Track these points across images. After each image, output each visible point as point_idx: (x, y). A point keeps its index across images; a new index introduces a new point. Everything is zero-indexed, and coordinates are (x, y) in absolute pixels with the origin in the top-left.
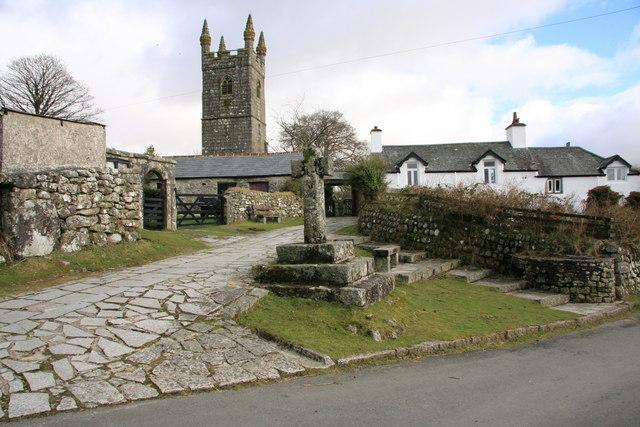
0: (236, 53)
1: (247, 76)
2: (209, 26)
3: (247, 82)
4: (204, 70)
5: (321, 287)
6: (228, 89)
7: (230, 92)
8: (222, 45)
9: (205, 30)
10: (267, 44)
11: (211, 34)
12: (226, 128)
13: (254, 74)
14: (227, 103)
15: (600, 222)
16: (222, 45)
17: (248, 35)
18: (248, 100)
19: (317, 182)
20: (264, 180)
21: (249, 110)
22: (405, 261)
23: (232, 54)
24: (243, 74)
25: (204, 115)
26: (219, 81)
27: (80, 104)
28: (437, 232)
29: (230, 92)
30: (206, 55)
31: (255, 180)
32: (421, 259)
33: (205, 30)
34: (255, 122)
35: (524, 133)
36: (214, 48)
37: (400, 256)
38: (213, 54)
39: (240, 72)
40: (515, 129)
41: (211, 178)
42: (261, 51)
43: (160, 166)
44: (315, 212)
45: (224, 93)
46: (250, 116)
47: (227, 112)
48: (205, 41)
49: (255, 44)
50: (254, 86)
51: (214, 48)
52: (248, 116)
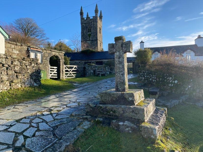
0: (92, 18)
4: (81, 24)
7: (90, 31)
8: (87, 15)
16: (87, 15)
17: (96, 11)
23: (91, 18)
30: (82, 19)
36: (85, 16)
45: (89, 32)
48: (81, 14)
51: (85, 16)
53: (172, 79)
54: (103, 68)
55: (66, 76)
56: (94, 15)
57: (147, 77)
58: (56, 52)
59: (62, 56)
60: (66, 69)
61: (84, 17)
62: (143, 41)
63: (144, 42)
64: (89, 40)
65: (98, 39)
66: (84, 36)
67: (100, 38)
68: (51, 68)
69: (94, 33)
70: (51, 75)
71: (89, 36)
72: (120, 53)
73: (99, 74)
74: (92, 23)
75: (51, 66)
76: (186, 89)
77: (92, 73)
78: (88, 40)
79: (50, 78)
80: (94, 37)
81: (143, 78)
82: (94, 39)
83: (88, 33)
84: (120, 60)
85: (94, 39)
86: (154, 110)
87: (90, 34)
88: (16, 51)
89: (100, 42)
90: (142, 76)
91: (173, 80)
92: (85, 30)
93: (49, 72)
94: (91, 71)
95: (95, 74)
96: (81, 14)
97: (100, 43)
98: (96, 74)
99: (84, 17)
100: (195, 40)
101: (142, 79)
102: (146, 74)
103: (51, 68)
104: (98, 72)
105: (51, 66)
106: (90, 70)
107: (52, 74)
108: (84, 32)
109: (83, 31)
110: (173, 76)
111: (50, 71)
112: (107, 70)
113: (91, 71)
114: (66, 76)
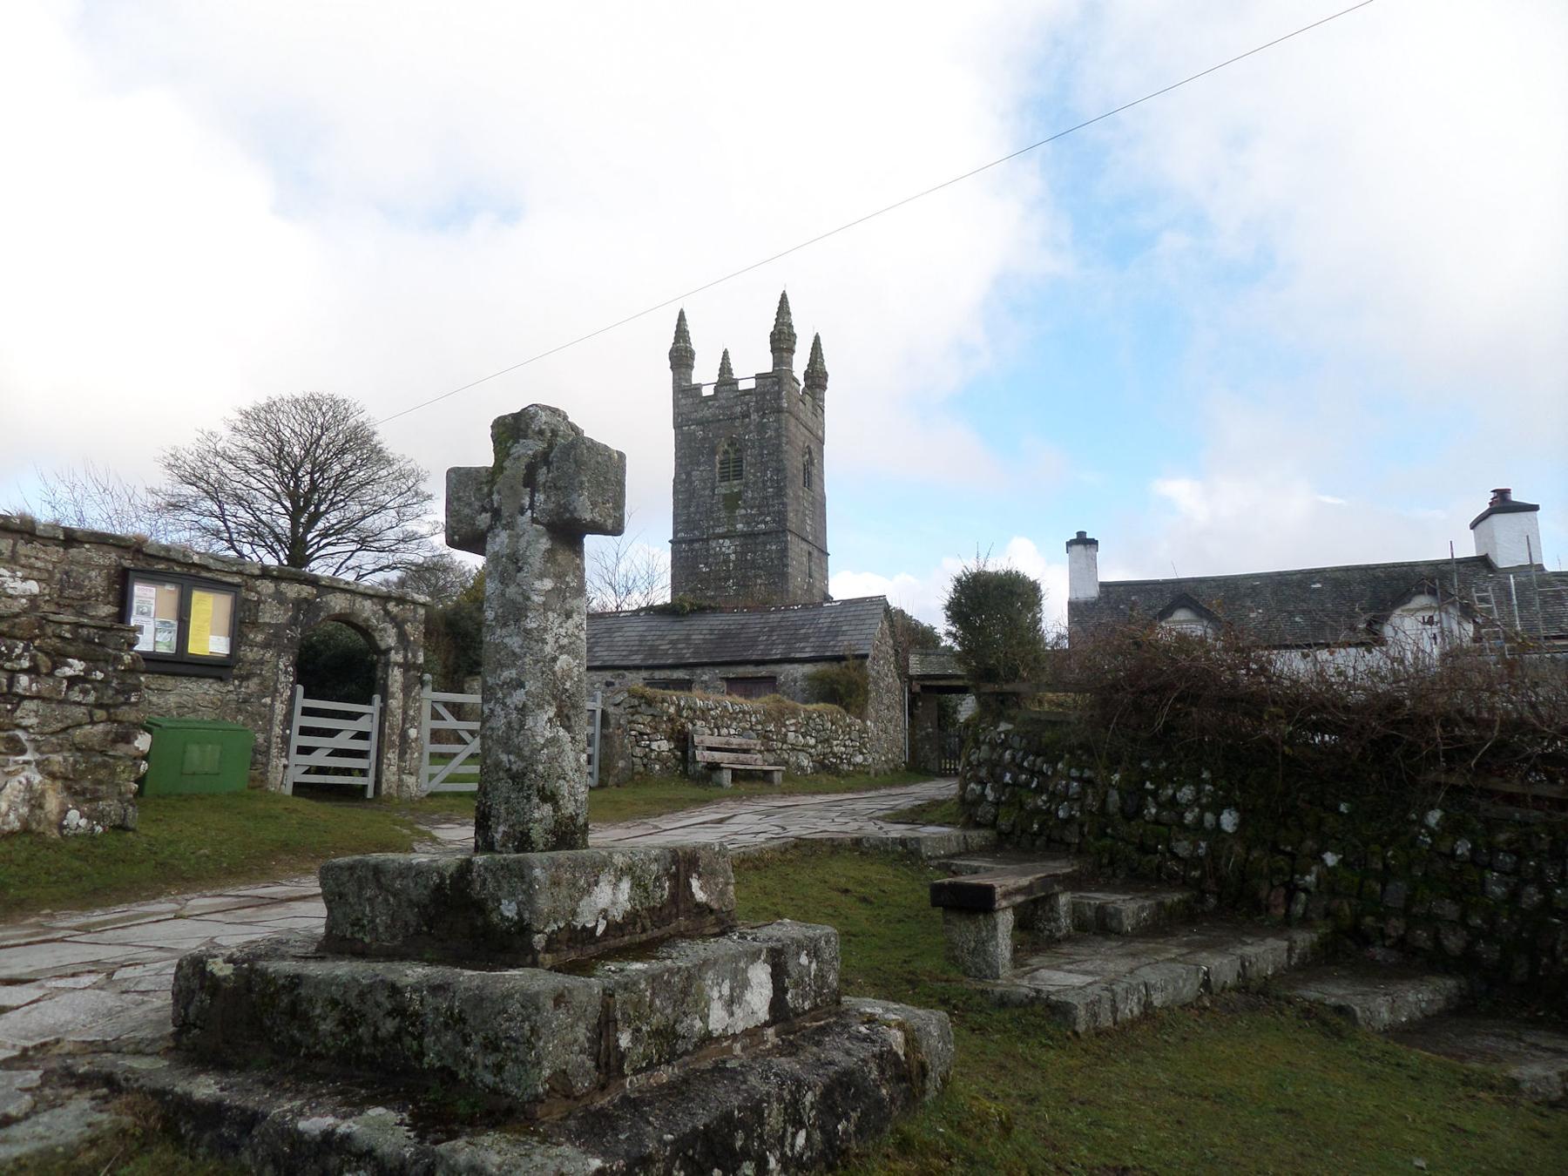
0: (751, 384)
1: (779, 436)
2: (691, 326)
3: (778, 448)
4: (677, 426)
5: (1070, 870)
6: (733, 469)
7: (739, 475)
8: (725, 368)
9: (681, 333)
10: (830, 365)
11: (696, 343)
12: (727, 561)
13: (800, 436)
14: (732, 501)
15: (559, 770)
16: (725, 368)
17: (782, 340)
18: (780, 492)
19: (536, 561)
20: (763, 671)
21: (781, 518)
22: (1099, 927)
23: (742, 386)
24: (770, 433)
25: (675, 532)
26: (713, 452)
27: (393, 513)
28: (1229, 820)
29: (739, 475)
30: (684, 391)
31: (741, 671)
32: (1158, 928)
33: (681, 333)
34: (797, 548)
35: (1536, 519)
36: (705, 375)
37: (1075, 909)
38: (698, 387)
39: (762, 428)
40: (1498, 520)
41: (627, 668)
42: (817, 377)
43: (367, 608)
44: (518, 697)
45: (724, 478)
46: (785, 531)
47: (732, 520)
48: (681, 357)
49: (800, 364)
50: (794, 462)
51: (705, 375)
52: (780, 531)
53: (1196, 801)
54: (758, 722)
55: (432, 777)
56: (767, 365)
57: (1015, 783)
58: (359, 599)
59: (408, 627)
60: (438, 724)
61: (695, 381)
62: (1089, 536)
63: (1094, 542)
64: (723, 536)
65: (791, 525)
66: (692, 509)
67: (804, 521)
68: (307, 712)
69: (765, 488)
70: (443, 771)
71: (726, 507)
72: (519, 536)
73: (714, 767)
74: (748, 416)
75: (305, 696)
76: (1308, 878)
77: (658, 759)
78: (719, 530)
79: (299, 788)
80: (761, 514)
81: (988, 791)
82: (766, 523)
83: (723, 489)
84: (512, 591)
85: (766, 523)
86: (139, 1035)
87: (739, 495)
88: (24, 579)
89: (805, 546)
90: (983, 772)
91: (1204, 809)
92: (698, 464)
93: (286, 740)
94: (654, 746)
95: (686, 768)
96: (681, 357)
97: (810, 553)
98: (690, 768)
99: (695, 381)
100: (1473, 526)
101: (983, 795)
102: (1008, 755)
103: (307, 712)
104: (707, 753)
105: (305, 696)
106: (641, 734)
107: (319, 759)
108: (691, 483)
109: (689, 474)
110: (1205, 775)
111: (296, 730)
112: (791, 735)
113: (654, 746)
114: (432, 777)
